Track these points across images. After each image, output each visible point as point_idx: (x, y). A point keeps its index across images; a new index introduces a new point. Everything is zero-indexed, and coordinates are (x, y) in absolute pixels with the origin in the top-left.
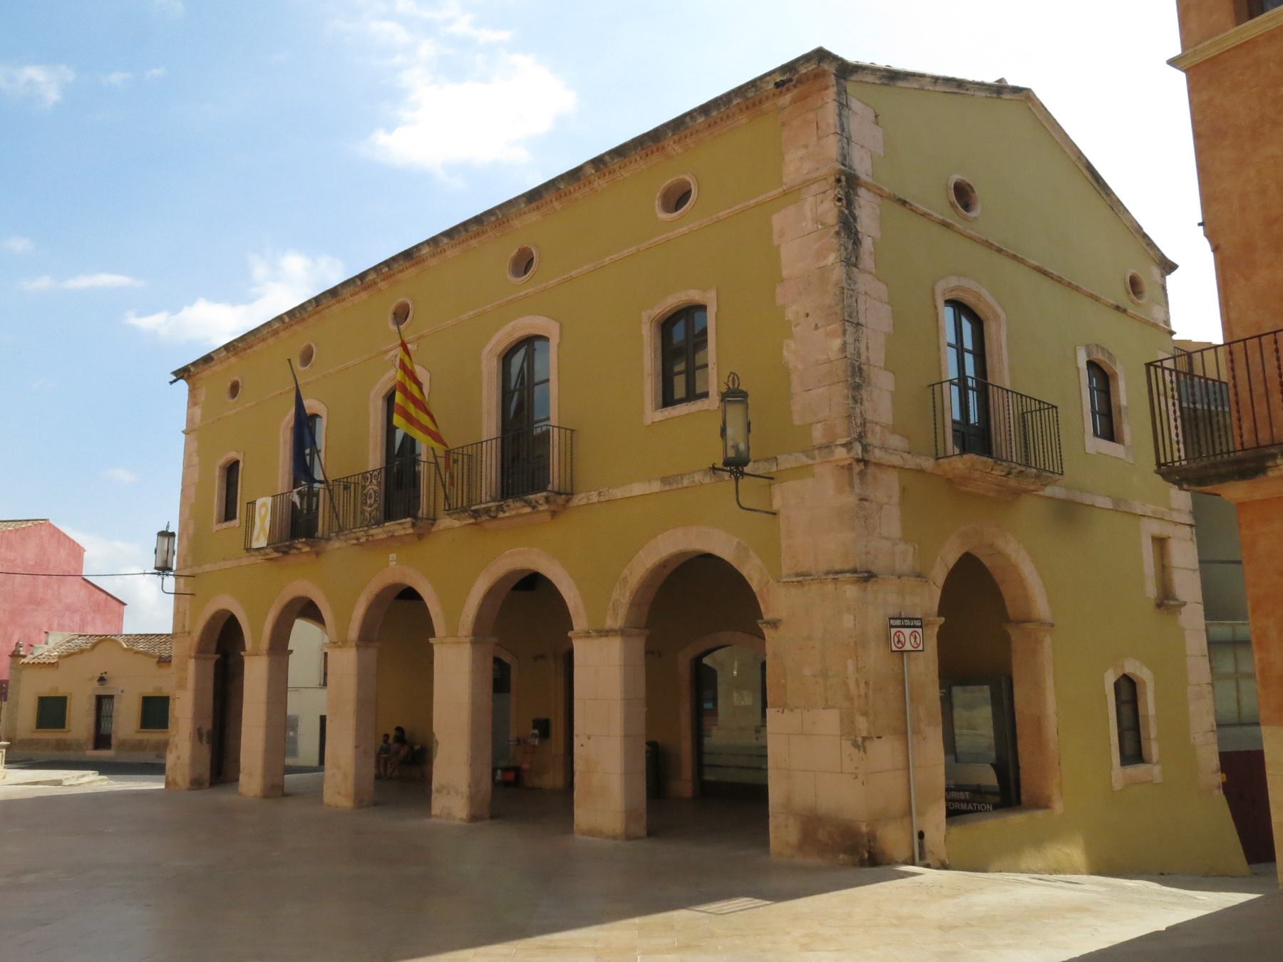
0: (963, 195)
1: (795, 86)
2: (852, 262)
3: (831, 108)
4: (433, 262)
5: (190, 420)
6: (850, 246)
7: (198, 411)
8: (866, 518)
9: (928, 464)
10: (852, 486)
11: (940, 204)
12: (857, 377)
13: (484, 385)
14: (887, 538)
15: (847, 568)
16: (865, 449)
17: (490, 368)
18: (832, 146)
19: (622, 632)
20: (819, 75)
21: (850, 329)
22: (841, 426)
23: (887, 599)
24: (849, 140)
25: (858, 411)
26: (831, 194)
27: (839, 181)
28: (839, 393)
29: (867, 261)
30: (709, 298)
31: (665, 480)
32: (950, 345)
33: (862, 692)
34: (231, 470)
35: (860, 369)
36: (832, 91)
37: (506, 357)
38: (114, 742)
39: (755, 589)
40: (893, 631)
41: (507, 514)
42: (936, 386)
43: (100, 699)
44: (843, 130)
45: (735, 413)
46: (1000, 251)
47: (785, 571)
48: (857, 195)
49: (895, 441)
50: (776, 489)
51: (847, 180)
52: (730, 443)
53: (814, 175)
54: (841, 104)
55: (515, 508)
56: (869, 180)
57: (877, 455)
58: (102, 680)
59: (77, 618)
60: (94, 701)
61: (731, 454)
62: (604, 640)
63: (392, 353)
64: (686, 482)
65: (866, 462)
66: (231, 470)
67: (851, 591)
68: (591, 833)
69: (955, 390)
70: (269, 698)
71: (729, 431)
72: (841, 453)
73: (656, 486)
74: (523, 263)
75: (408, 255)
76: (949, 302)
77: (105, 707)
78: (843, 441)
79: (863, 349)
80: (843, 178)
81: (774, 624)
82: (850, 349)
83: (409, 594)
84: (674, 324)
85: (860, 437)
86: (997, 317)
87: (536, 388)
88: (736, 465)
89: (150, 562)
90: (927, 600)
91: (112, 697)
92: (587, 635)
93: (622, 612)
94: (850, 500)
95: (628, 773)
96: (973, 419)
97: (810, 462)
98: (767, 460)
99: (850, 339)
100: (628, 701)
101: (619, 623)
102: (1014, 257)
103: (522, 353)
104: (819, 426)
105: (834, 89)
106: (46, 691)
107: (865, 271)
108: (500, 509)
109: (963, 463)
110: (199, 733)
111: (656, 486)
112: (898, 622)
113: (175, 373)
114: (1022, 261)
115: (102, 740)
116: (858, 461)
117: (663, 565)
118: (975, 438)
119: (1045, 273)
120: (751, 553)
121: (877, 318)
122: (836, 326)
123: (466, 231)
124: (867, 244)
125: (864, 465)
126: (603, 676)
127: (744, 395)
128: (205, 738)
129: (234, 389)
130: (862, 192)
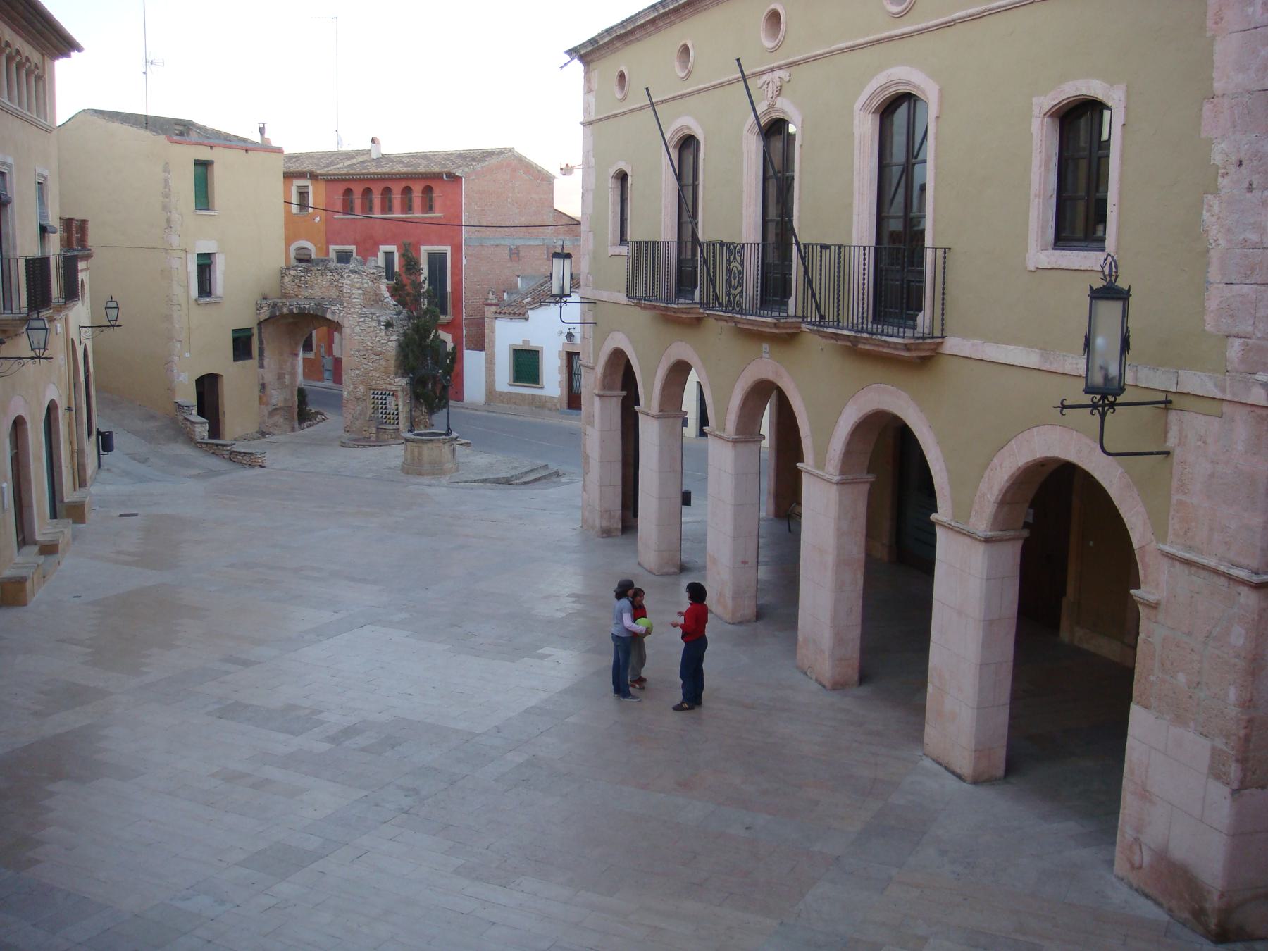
7: (592, 99)
13: (856, 153)
30: (1113, 96)
39: (1135, 545)
45: (1109, 309)
50: (1173, 416)
52: (1098, 361)
60: (564, 356)
61: (1098, 379)
71: (1099, 342)
84: (1080, 117)
100: (989, 624)
103: (905, 106)
104: (1237, 342)
127: (1122, 296)
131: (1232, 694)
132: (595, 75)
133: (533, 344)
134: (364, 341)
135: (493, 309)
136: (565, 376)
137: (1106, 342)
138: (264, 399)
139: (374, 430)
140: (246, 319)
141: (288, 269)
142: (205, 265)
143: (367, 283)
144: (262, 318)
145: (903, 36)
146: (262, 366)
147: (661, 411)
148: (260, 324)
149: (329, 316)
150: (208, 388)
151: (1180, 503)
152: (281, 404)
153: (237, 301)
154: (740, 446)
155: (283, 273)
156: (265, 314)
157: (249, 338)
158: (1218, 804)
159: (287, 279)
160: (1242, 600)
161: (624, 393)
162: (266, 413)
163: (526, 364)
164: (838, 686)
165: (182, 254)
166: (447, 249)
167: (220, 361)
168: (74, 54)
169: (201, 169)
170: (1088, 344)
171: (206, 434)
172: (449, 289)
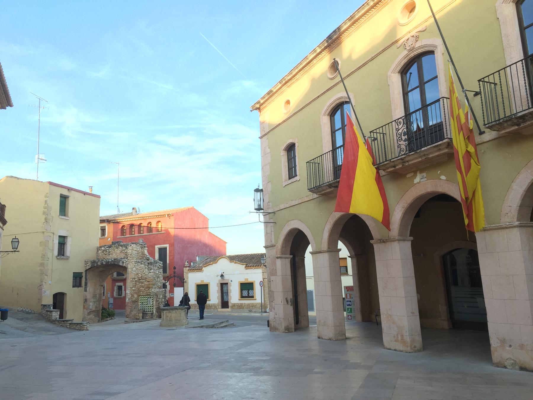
8: (42, 265)
34: (291, 148)
37: (404, 71)
38: (230, 305)
43: (222, 285)
58: (222, 276)
60: (219, 285)
87: (341, 126)
89: (252, 206)
91: (227, 284)
115: (225, 304)
128: (290, 303)
133: (205, 282)
134: (137, 274)
135: (188, 268)
136: (220, 294)
138: (86, 307)
139: (141, 315)
140: (80, 268)
141: (101, 247)
142: (62, 242)
143: (139, 248)
144: (88, 268)
146: (86, 291)
147: (329, 248)
148: (86, 271)
149: (121, 264)
150: (59, 299)
152: (94, 309)
153: (76, 262)
154: (401, 242)
155: (98, 249)
156: (89, 266)
157: (81, 278)
159: (100, 252)
161: (292, 256)
162: (86, 313)
165: (52, 235)
167: (65, 285)
168: (8, 108)
169: (63, 199)
171: (58, 317)
172: (168, 262)
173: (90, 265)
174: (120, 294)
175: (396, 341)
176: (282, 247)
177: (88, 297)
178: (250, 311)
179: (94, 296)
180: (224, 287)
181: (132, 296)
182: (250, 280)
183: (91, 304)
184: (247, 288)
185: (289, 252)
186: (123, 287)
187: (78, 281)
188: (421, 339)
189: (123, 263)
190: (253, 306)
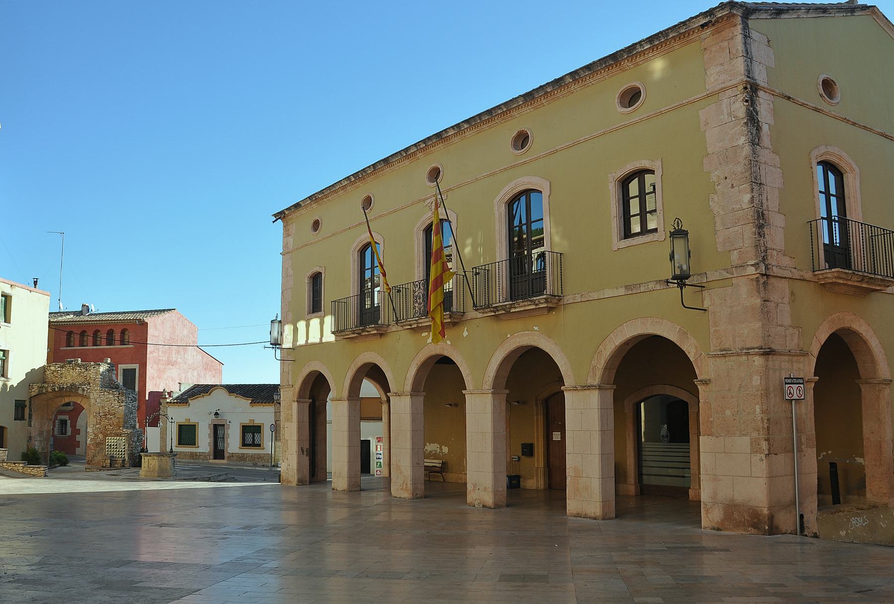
0: (828, 86)
1: (713, 25)
2: (755, 141)
3: (739, 39)
4: (456, 139)
5: (285, 246)
6: (754, 132)
9: (808, 275)
10: (759, 292)
11: (813, 95)
12: (761, 220)
14: (781, 326)
15: (756, 346)
16: (767, 268)
17: (500, 211)
18: (740, 64)
19: (600, 388)
20: (731, 16)
21: (756, 187)
22: (751, 252)
23: (784, 367)
24: (751, 59)
25: (762, 242)
26: (741, 97)
27: (746, 88)
28: (749, 231)
29: (766, 140)
31: (627, 287)
32: (821, 192)
33: (766, 426)
34: (316, 279)
35: (763, 214)
36: (739, 27)
37: (511, 203)
38: (226, 455)
40: (787, 386)
41: (517, 310)
42: (812, 225)
43: (216, 428)
44: (747, 53)
45: (679, 244)
46: (854, 124)
47: (712, 348)
48: (757, 96)
49: (786, 261)
50: (706, 293)
51: (751, 88)
52: (677, 265)
53: (729, 84)
54: (745, 36)
55: (522, 306)
56: (766, 85)
57: (775, 271)
58: (216, 414)
59: (195, 374)
61: (678, 272)
62: (588, 392)
63: (428, 201)
64: (642, 289)
65: (768, 276)
66: (316, 279)
67: (758, 361)
68: (578, 515)
69: (825, 222)
70: (349, 428)
72: (751, 270)
73: (622, 291)
74: (522, 140)
75: (438, 135)
76: (819, 163)
77: (220, 432)
78: (753, 262)
79: (764, 201)
80: (749, 86)
81: (706, 382)
82: (756, 201)
83: (444, 361)
85: (764, 259)
86: (852, 170)
88: (681, 279)
90: (807, 368)
92: (575, 389)
93: (599, 373)
94: (758, 301)
95: (603, 478)
96: (837, 240)
97: (730, 276)
98: (700, 274)
99: (756, 195)
100: (603, 431)
101: (596, 382)
102: (865, 128)
105: (741, 26)
106: (182, 421)
107: (763, 148)
108: (511, 306)
109: (831, 274)
110: (301, 450)
111: (622, 291)
112: (789, 381)
113: (275, 215)
114: (870, 130)
115: (218, 453)
116: (763, 275)
117: (626, 343)
118: (838, 255)
119: (886, 137)
120: (689, 336)
121: (772, 178)
122: (746, 186)
123: (480, 119)
124: (765, 128)
125: (766, 278)
126: (585, 417)
129: (316, 225)
130: (761, 93)
131: (758, 409)
132: (293, 228)
133: (193, 421)
137: (679, 257)
144: (33, 394)
145: (524, 163)
146: (30, 425)
151: (716, 331)
158: (760, 467)
160: (756, 363)
163: (187, 434)
164: (497, 506)
166: (136, 366)
170: (672, 257)
173: (37, 391)
174: (63, 431)
175: (402, 489)
176: (301, 390)
177: (33, 435)
178: (255, 465)
179: (41, 433)
180: (218, 430)
181: (96, 435)
182: (257, 422)
183: (36, 443)
184: (251, 432)
185: (308, 396)
186: (69, 422)
187: (20, 411)
188: (423, 487)
189: (84, 390)
190: (260, 457)
